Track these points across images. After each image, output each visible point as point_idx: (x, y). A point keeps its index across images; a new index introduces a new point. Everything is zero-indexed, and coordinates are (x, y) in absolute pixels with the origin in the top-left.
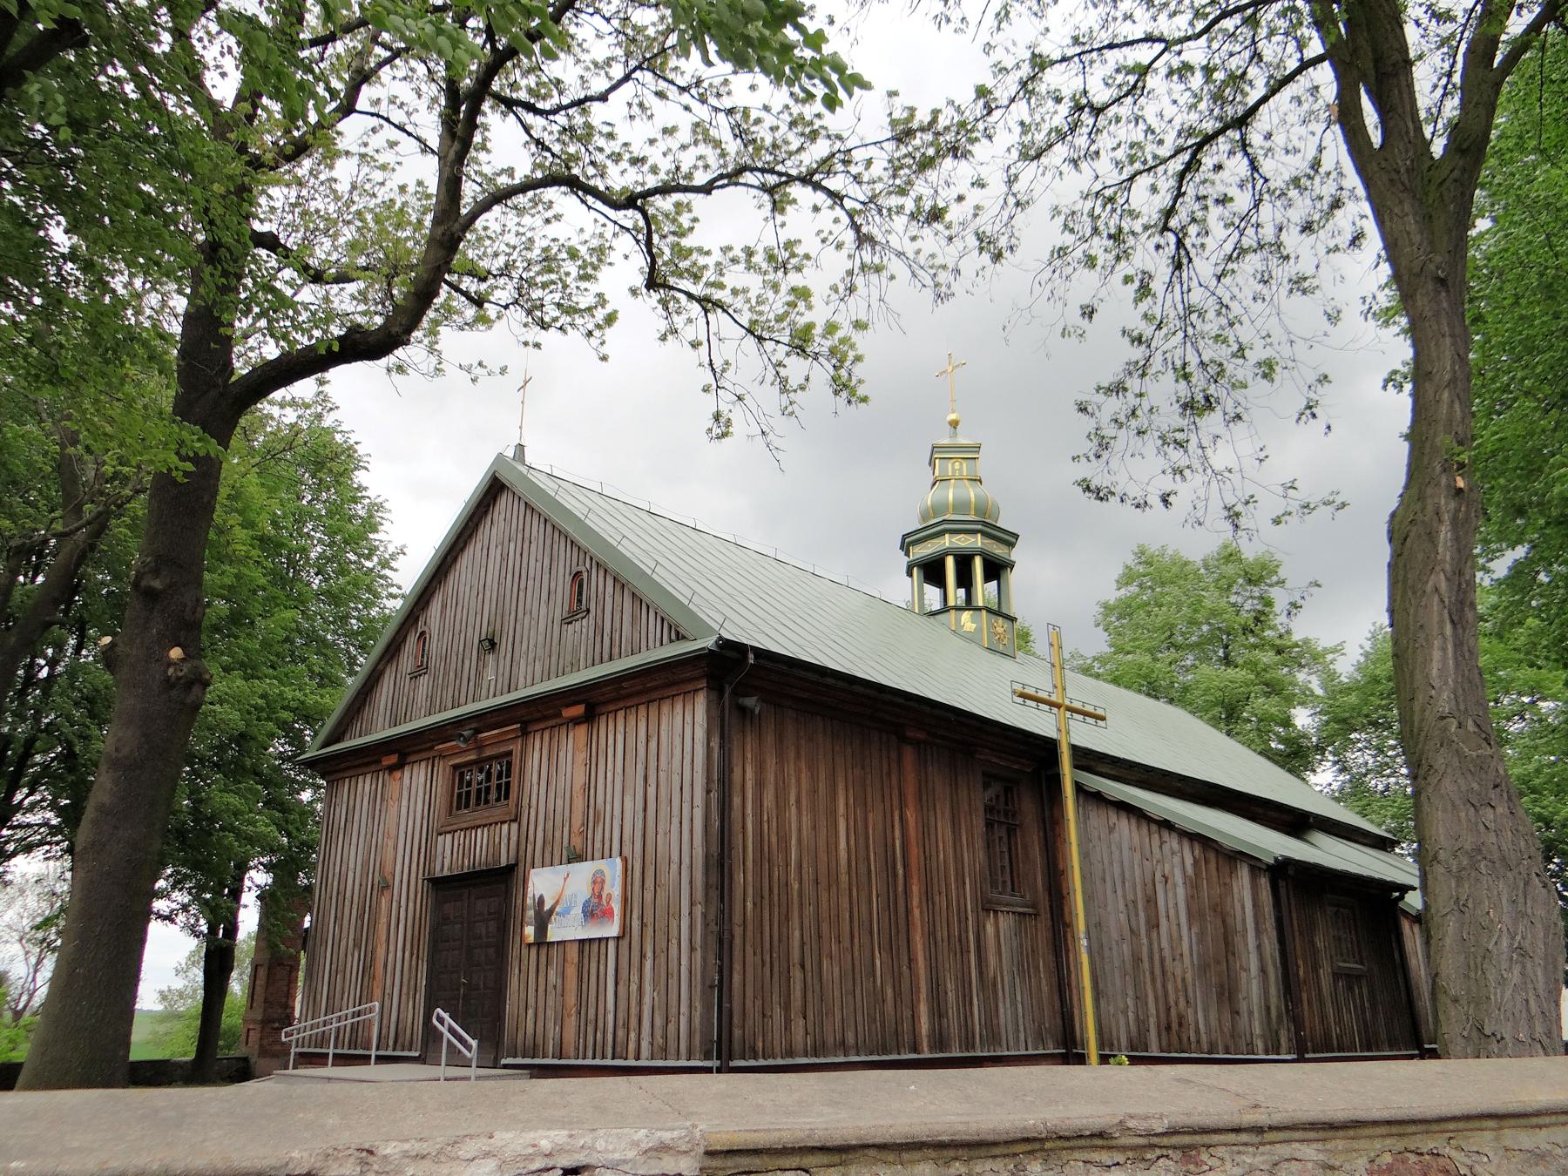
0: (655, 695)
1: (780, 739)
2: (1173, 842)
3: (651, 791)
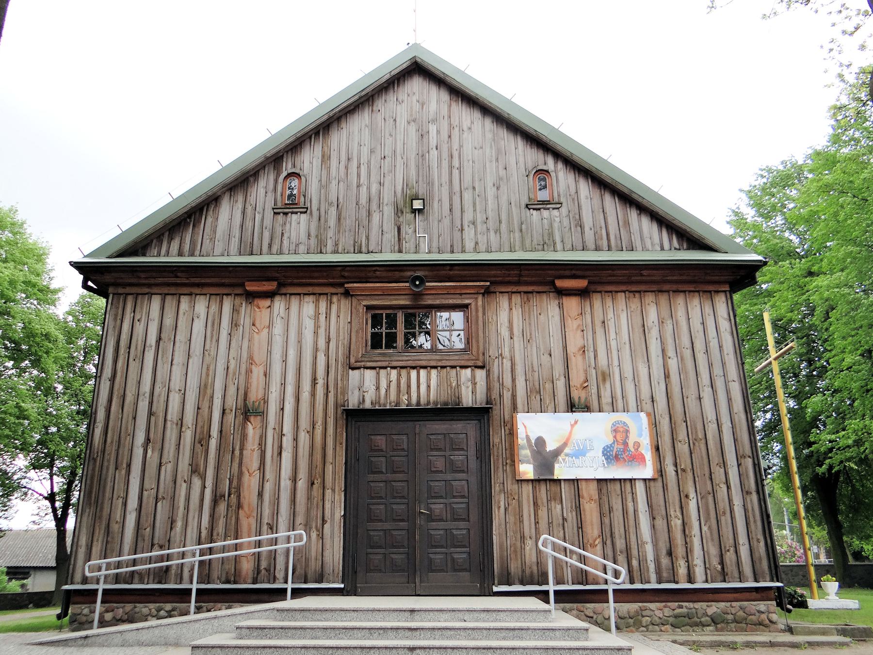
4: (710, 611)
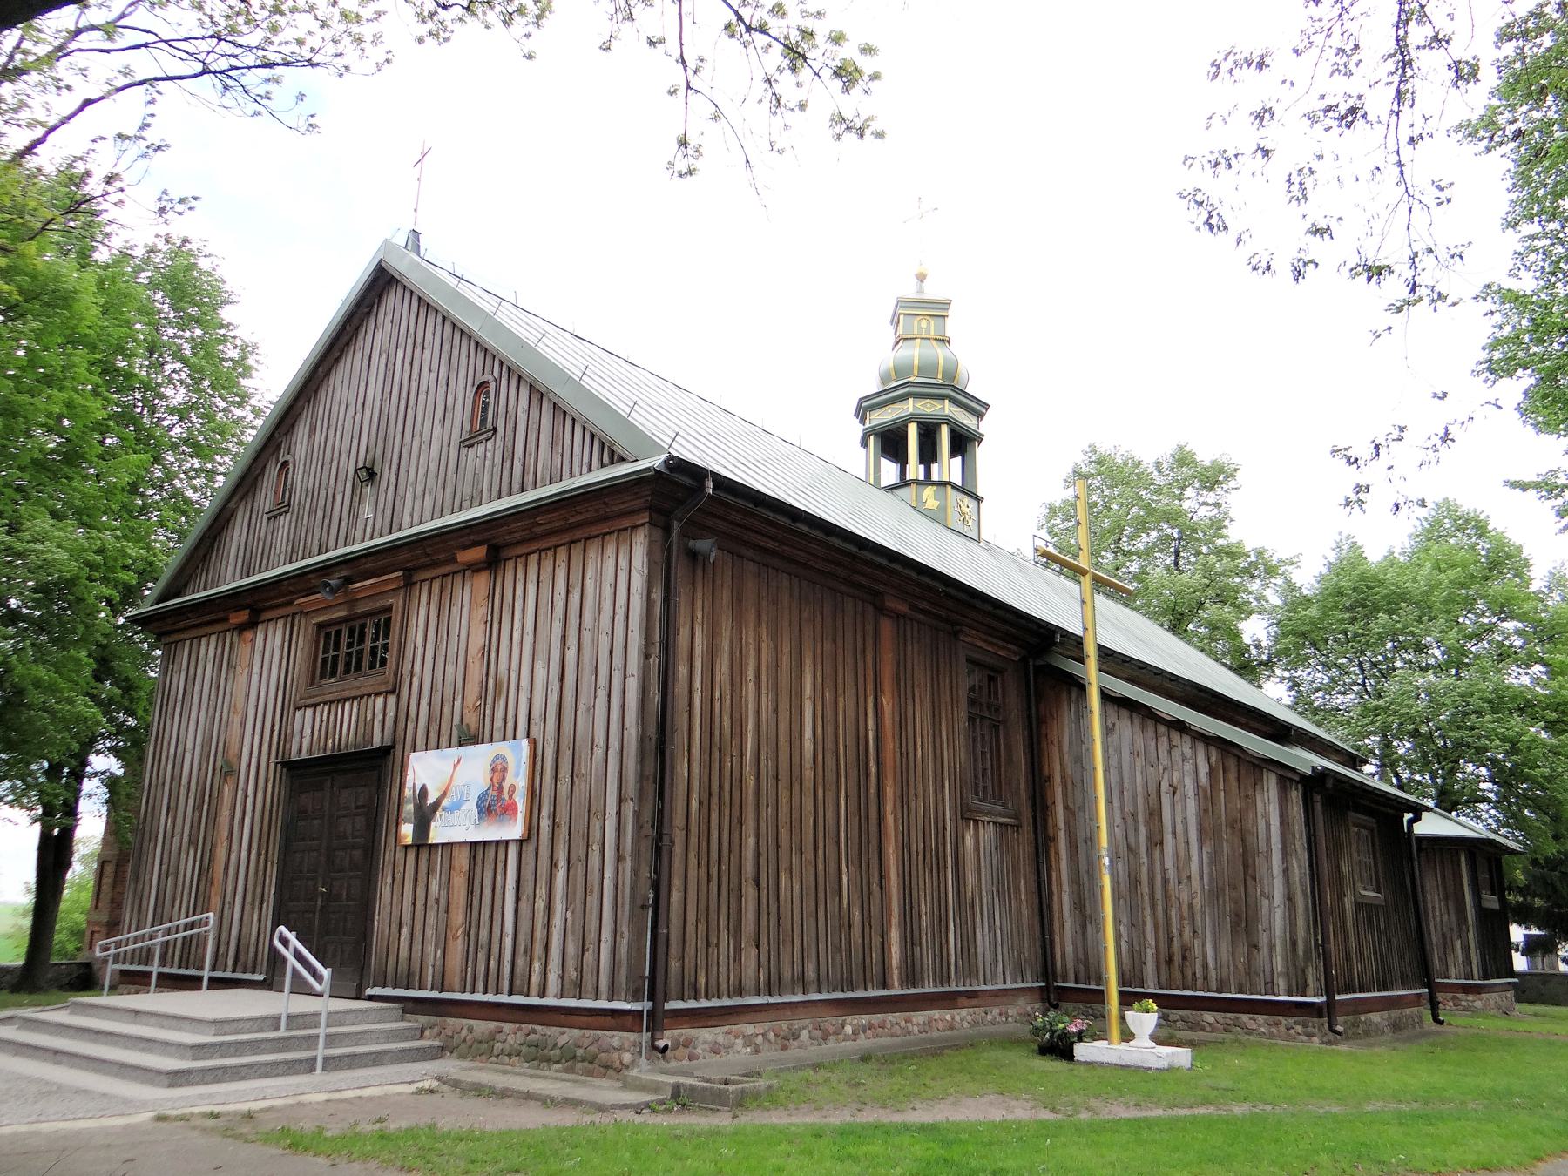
0: (578, 534)
1: (737, 600)
2: (1185, 745)
3: (571, 656)
4: (561, 1041)
